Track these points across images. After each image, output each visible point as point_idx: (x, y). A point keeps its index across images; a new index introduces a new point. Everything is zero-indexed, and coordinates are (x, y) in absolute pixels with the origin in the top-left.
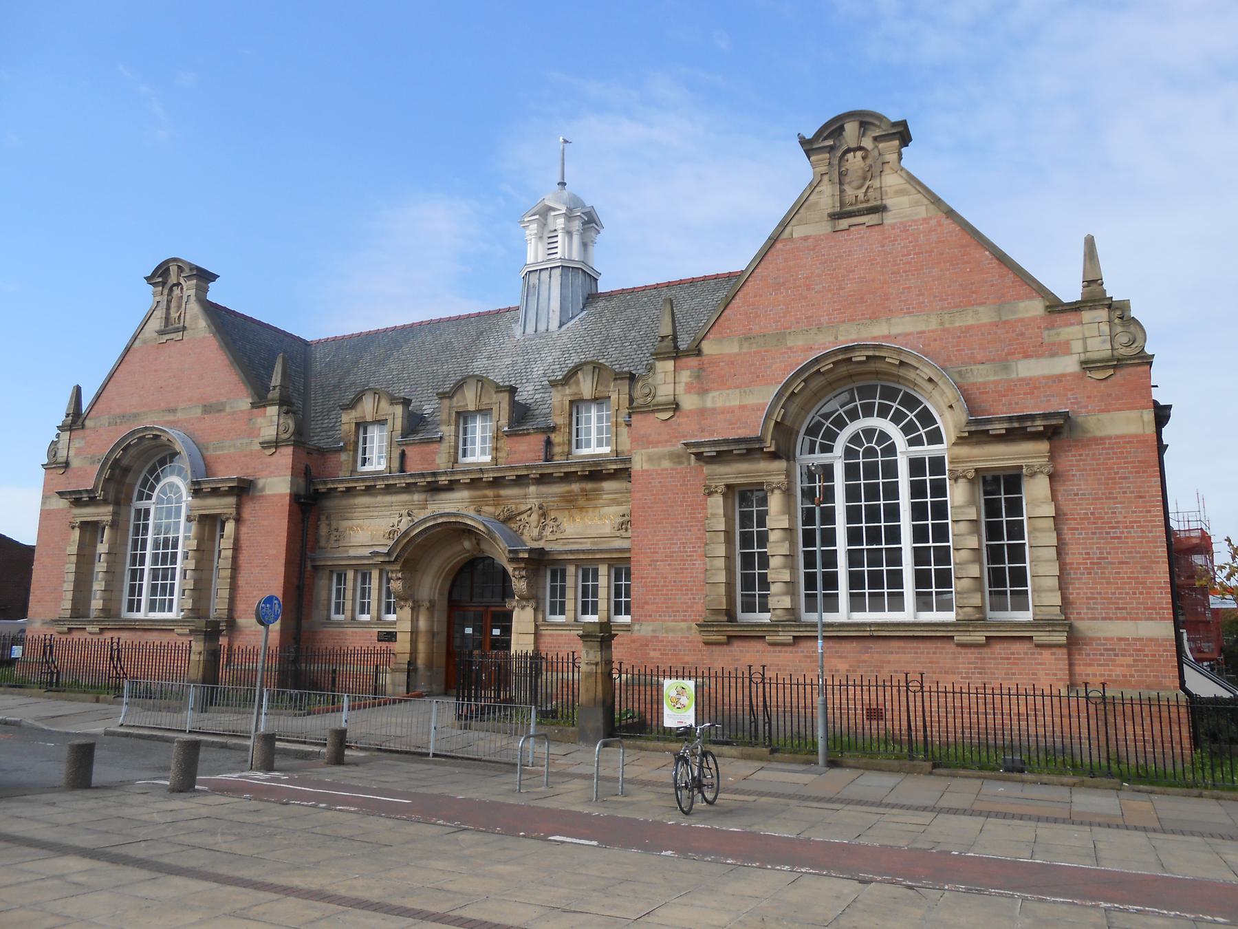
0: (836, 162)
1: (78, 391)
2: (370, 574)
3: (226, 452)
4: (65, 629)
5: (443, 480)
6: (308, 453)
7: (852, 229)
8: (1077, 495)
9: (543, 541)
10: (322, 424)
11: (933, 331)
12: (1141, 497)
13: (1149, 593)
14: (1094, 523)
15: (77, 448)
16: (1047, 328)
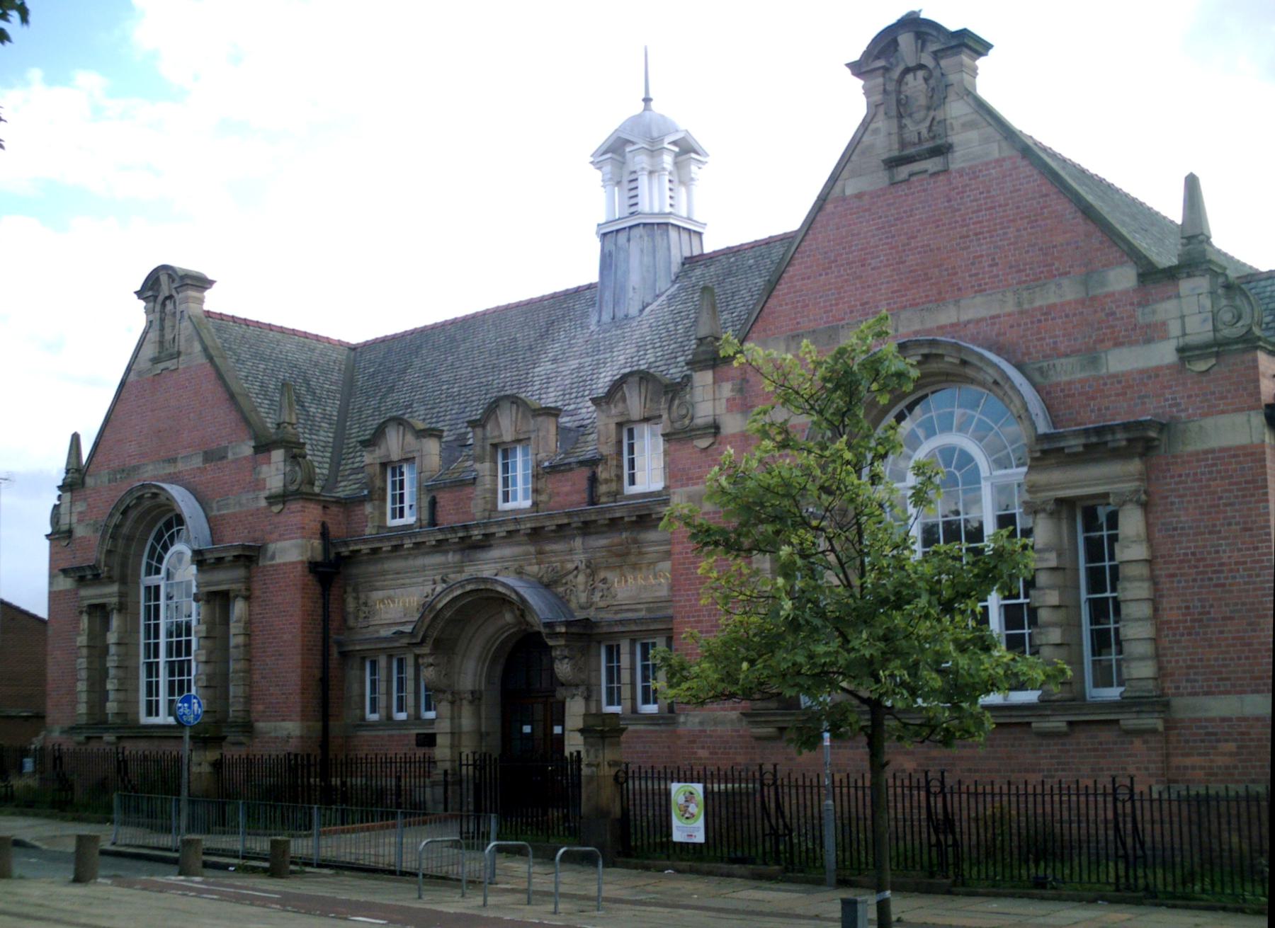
0: (891, 87)
1: (76, 439)
2: (618, 646)
3: (230, 511)
4: (82, 738)
5: (476, 534)
6: (324, 507)
7: (914, 179)
8: (1175, 529)
9: (593, 609)
10: (353, 463)
11: (1009, 315)
12: (1246, 530)
13: (1255, 658)
14: (1196, 567)
15: (80, 513)
16: (1139, 304)
